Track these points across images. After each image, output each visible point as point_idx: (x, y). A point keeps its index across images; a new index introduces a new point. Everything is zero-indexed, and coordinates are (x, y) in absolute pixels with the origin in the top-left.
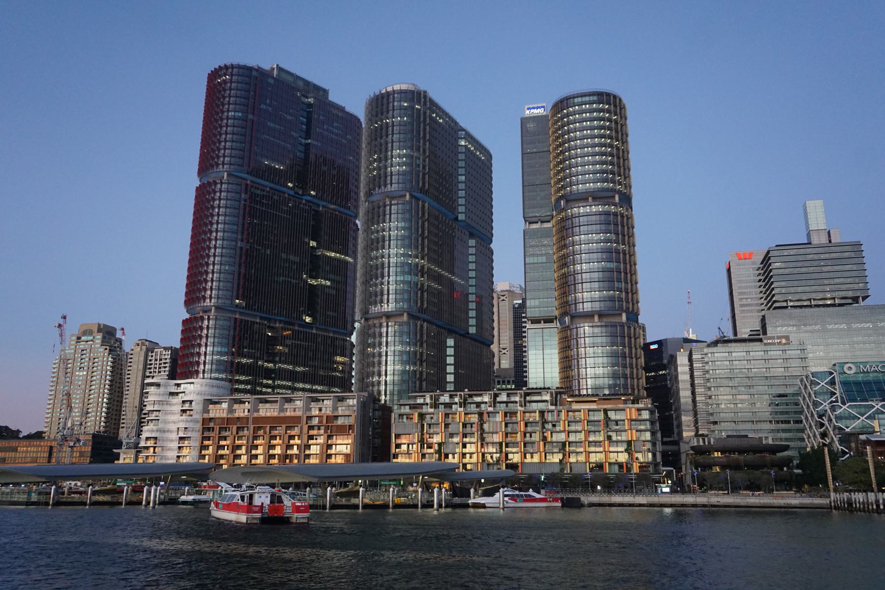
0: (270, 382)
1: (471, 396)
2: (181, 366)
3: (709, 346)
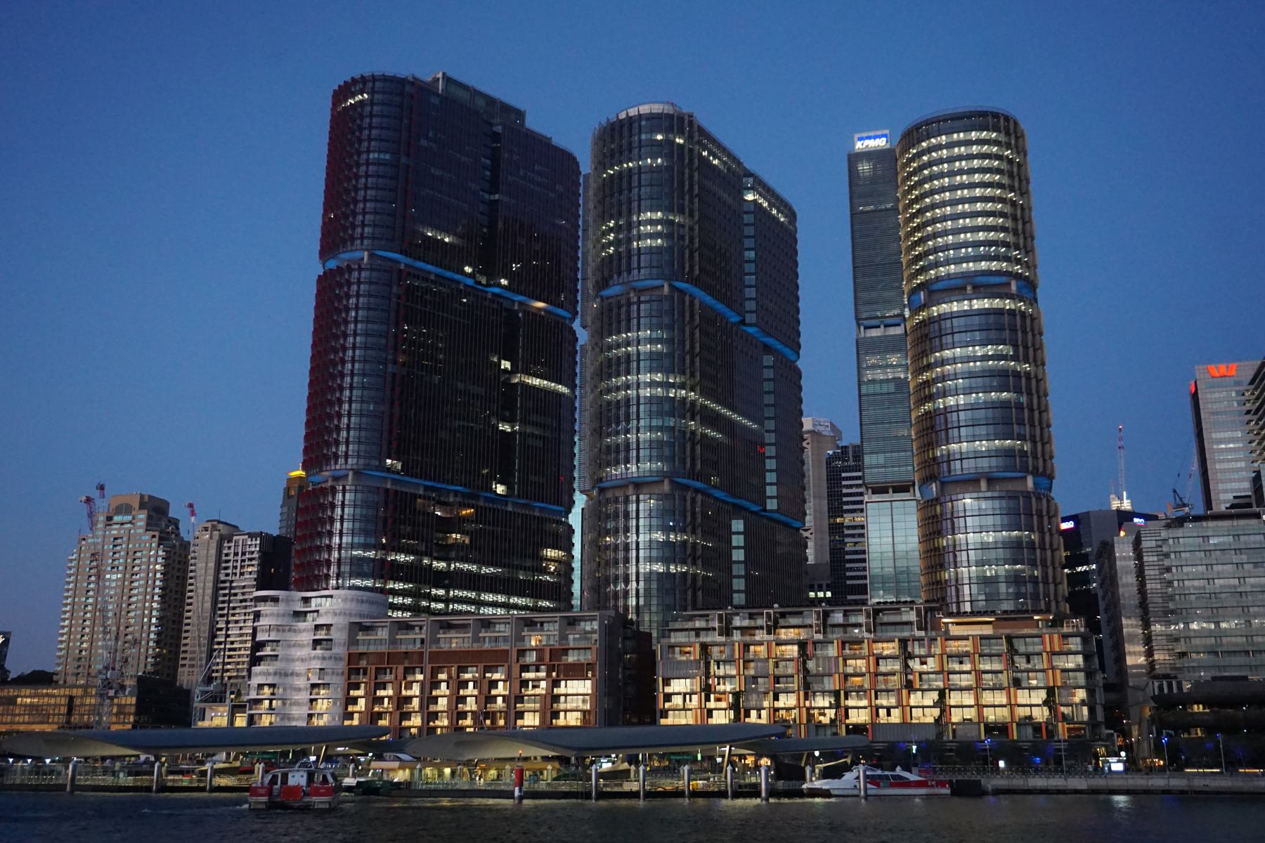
1: (783, 615)
2: (288, 562)
3: (1168, 526)
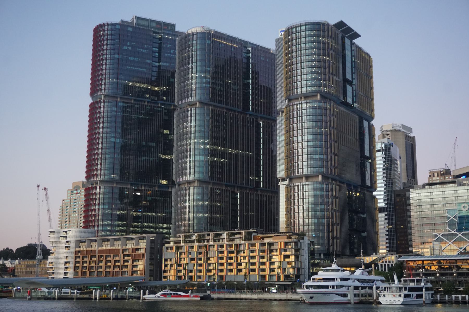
0: (153, 225)
